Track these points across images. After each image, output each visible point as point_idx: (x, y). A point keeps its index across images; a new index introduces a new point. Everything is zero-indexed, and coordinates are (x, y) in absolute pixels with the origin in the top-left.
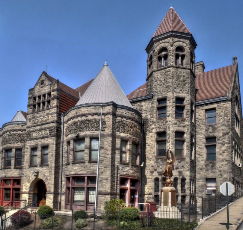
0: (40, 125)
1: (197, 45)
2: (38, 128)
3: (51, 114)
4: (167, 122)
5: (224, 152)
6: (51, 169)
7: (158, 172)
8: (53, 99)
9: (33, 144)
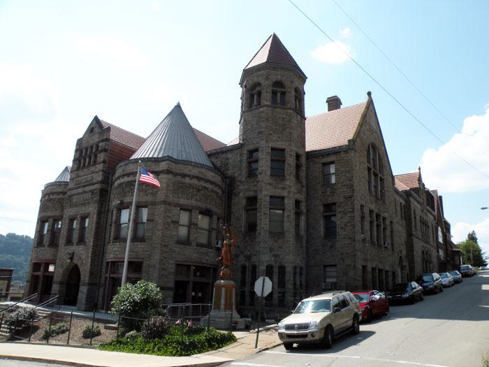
0: (83, 187)
1: (101, 150)
2: (80, 190)
3: (97, 172)
4: (258, 182)
5: (346, 225)
6: (88, 248)
7: (245, 256)
8: (101, 152)
9: (71, 214)
